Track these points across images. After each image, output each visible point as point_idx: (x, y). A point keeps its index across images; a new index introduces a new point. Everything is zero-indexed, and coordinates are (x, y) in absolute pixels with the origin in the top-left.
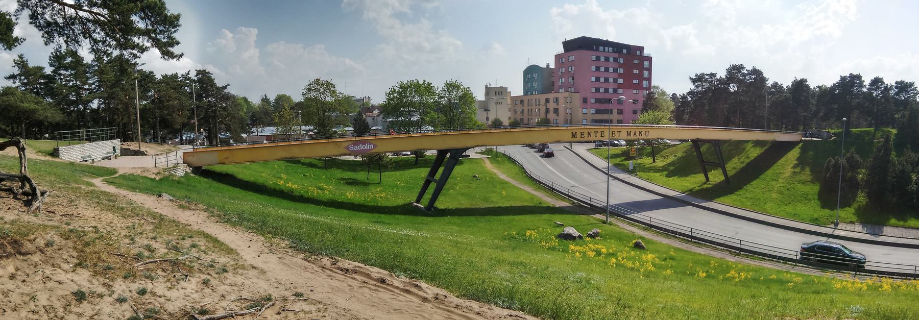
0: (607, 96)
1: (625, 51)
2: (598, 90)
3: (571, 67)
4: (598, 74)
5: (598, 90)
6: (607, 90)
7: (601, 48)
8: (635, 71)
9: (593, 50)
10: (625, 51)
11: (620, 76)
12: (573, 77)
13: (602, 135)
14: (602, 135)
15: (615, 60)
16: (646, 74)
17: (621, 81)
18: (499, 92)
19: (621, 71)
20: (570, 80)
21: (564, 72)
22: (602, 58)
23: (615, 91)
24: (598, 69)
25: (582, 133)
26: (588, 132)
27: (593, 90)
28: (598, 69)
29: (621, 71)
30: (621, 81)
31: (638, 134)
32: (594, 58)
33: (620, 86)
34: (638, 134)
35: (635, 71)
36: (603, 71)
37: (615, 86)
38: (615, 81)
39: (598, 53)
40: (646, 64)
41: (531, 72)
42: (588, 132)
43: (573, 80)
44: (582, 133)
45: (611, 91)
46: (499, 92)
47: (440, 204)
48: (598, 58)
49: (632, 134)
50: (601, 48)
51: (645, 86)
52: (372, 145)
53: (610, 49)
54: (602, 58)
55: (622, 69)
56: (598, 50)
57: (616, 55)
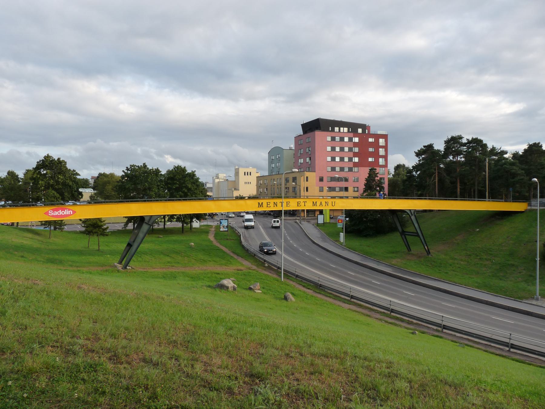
0: (343, 175)
1: (360, 131)
2: (333, 169)
3: (309, 148)
4: (333, 154)
5: (333, 169)
6: (342, 169)
7: (337, 129)
8: (371, 150)
9: (328, 130)
10: (360, 131)
11: (355, 155)
12: (310, 158)
13: (268, 206)
14: (288, 205)
15: (350, 140)
16: (382, 152)
17: (356, 160)
18: (248, 173)
19: (356, 150)
20: (308, 160)
21: (302, 153)
22: (338, 139)
23: (350, 170)
24: (333, 149)
25: (288, 203)
26: (274, 203)
27: (329, 169)
28: (333, 149)
29: (356, 150)
30: (356, 160)
31: (324, 204)
32: (329, 139)
33: (356, 165)
34: (324, 204)
35: (371, 150)
36: (339, 150)
37: (351, 165)
38: (350, 159)
39: (333, 134)
40: (382, 142)
41: (368, 177)
42: (274, 203)
43: (310, 160)
44: (299, 203)
45: (346, 169)
46: (248, 173)
47: (416, 232)
48: (333, 139)
49: (318, 204)
50: (337, 129)
51: (380, 164)
52: (71, 211)
53: (346, 130)
54: (338, 139)
55: (358, 148)
56: (333, 130)
57: (351, 135)
